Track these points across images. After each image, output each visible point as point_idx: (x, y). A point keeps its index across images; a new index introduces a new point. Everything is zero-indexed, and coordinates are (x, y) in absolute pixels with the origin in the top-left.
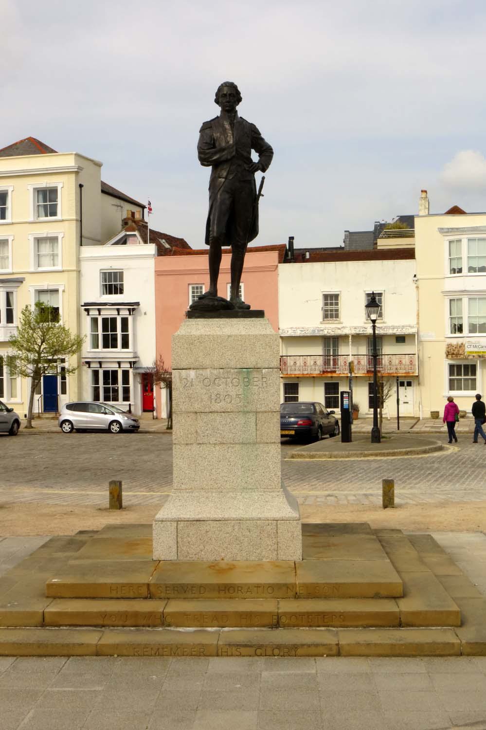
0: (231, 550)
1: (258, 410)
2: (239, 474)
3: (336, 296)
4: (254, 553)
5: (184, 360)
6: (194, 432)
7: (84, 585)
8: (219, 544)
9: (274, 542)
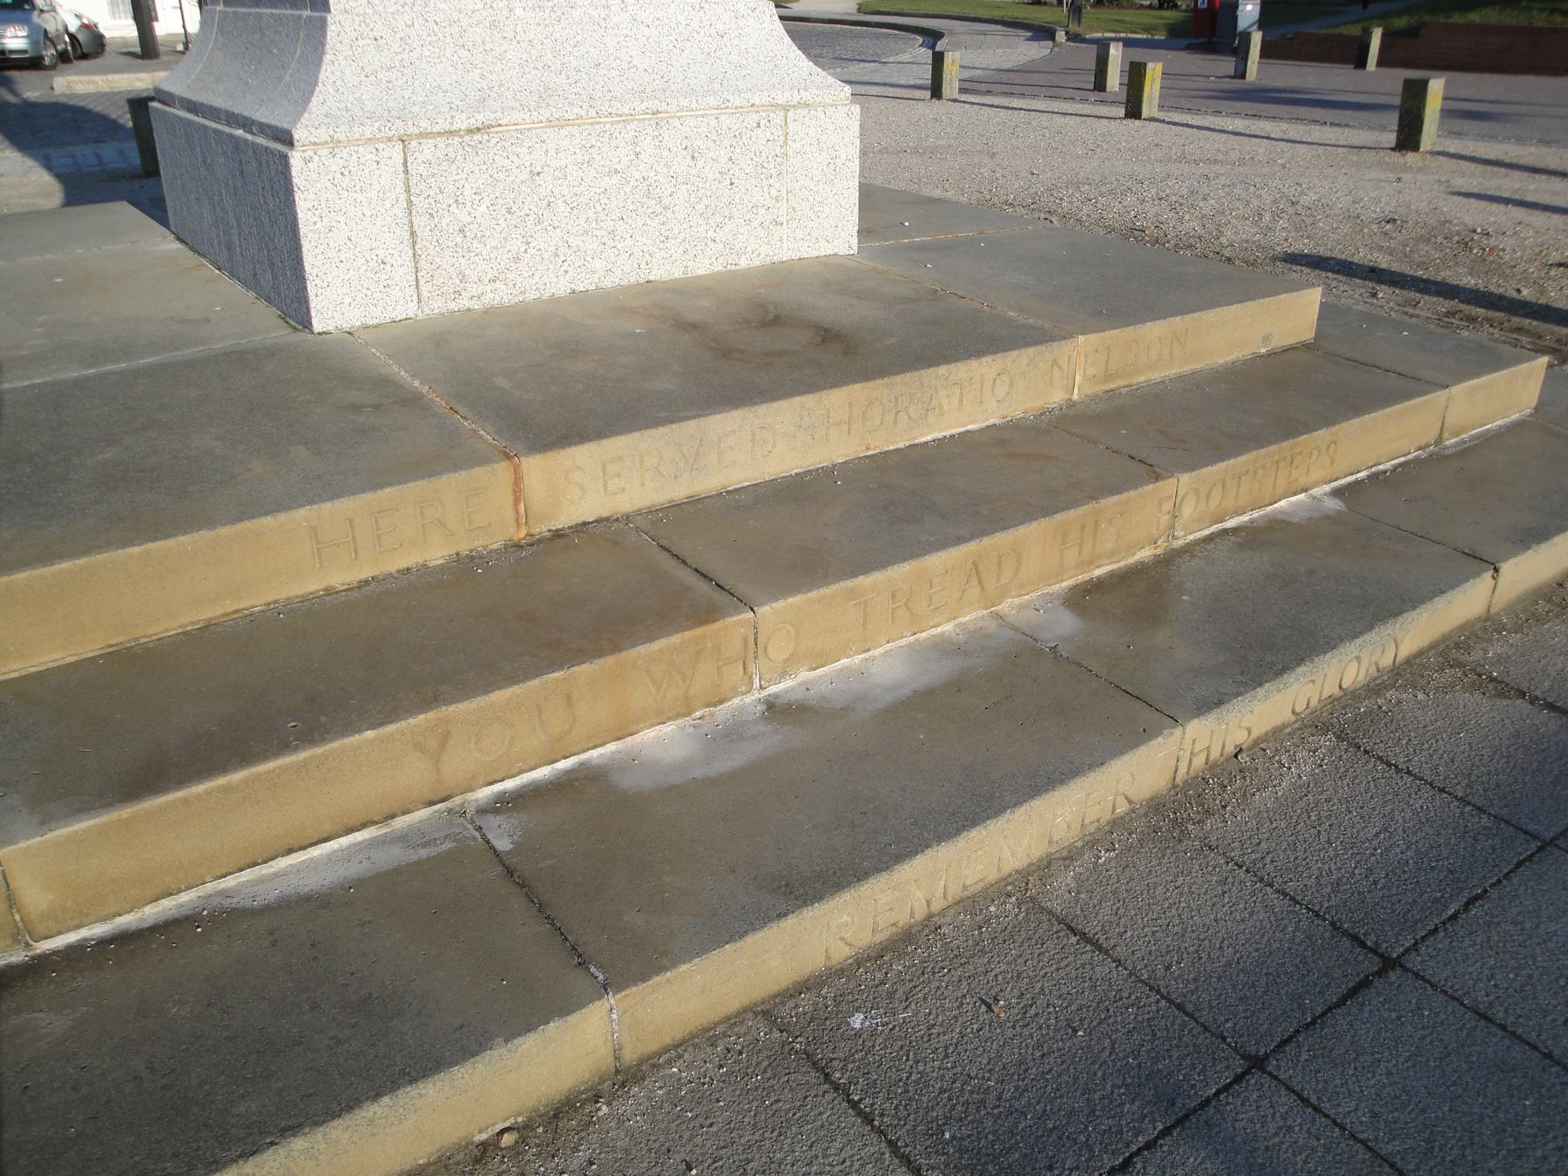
0: (629, 242)
4: (711, 244)
8: (582, 221)
9: (774, 193)
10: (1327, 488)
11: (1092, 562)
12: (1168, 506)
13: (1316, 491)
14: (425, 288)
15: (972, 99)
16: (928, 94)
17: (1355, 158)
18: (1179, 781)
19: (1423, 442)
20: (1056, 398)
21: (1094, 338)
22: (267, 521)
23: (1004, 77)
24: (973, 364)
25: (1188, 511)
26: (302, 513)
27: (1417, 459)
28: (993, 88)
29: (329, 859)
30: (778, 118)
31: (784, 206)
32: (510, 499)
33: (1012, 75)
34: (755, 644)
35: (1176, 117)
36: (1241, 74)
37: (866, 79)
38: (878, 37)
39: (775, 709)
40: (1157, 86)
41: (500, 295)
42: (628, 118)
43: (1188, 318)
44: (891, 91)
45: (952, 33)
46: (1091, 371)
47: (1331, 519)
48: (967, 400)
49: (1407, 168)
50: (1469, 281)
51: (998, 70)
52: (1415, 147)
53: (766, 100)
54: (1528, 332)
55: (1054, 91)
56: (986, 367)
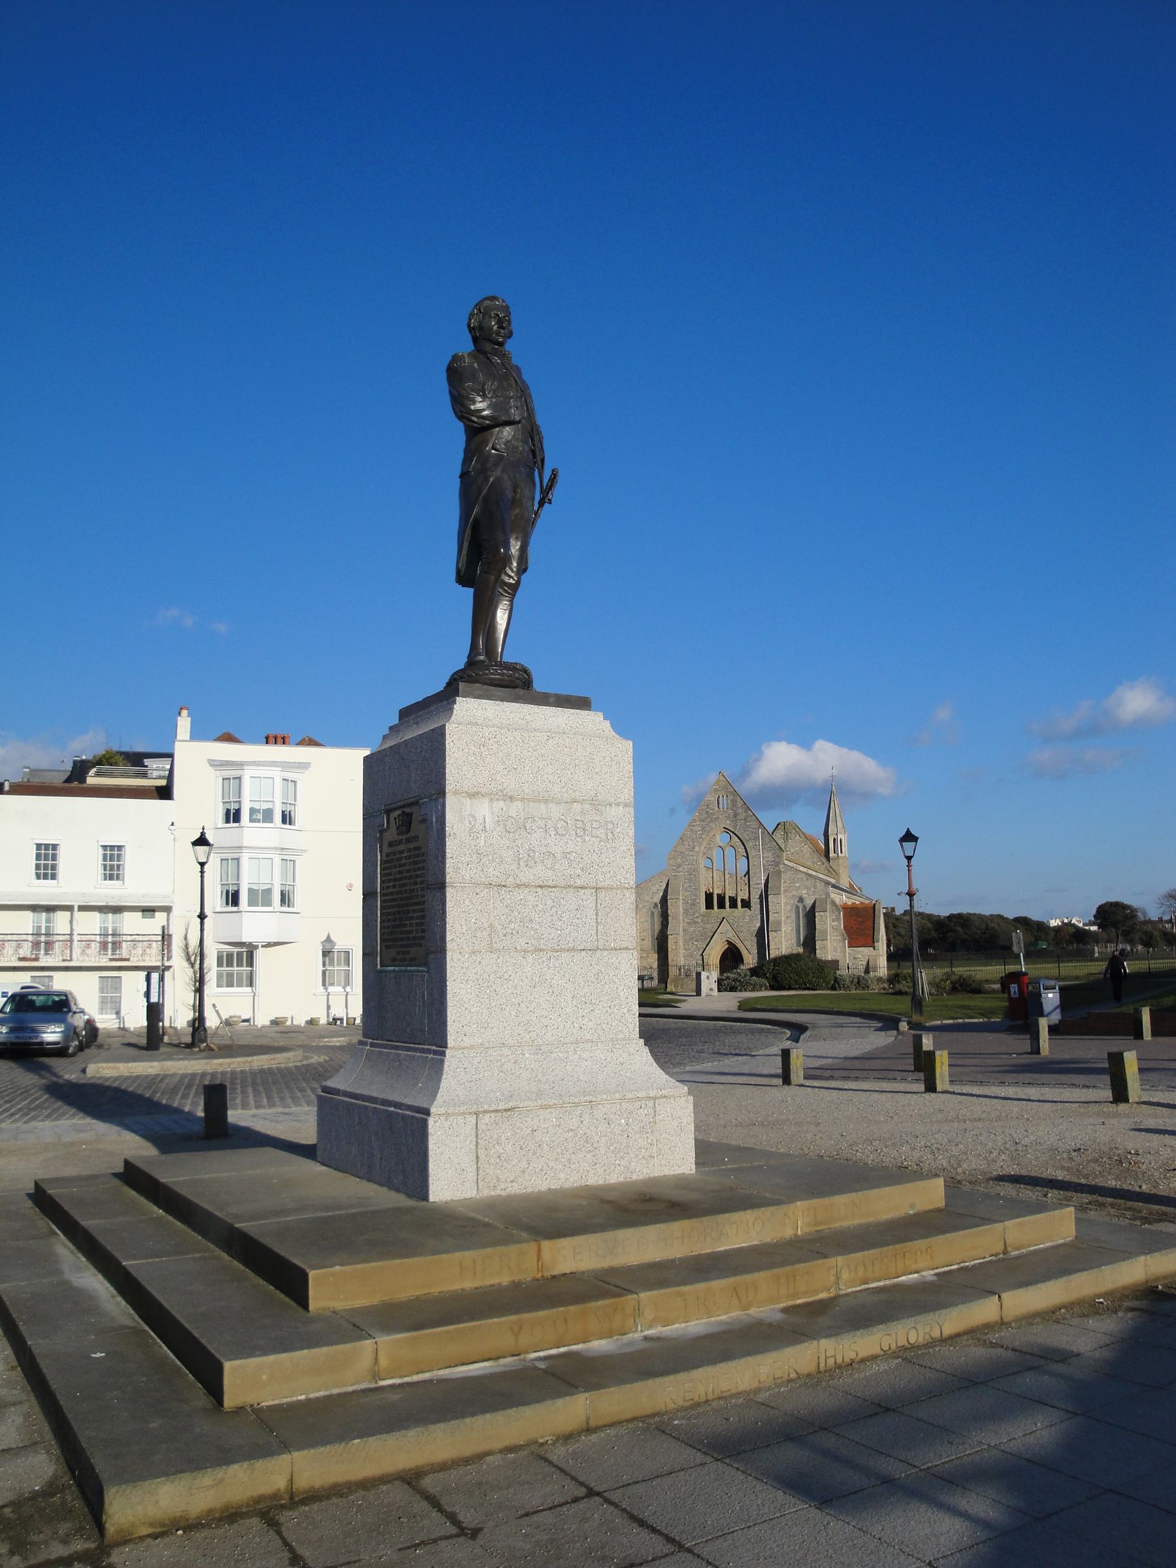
1: (600, 885)
2: (568, 1010)
3: (55, 847)
5: (469, 776)
6: (486, 925)
7: (5, 1307)
10: (932, 1272)
11: (795, 1296)
12: (833, 1272)
13: (924, 1273)
14: (481, 1184)
15: (816, 1083)
16: (780, 1081)
17: (1082, 1110)
18: (822, 1369)
19: (994, 1252)
20: (788, 1233)
21: (806, 1203)
22: (445, 1256)
23: (848, 1064)
24: (742, 1213)
25: (845, 1275)
26: (458, 1254)
27: (991, 1262)
28: (836, 1074)
29: (484, 1368)
30: (651, 1104)
31: (655, 1148)
32: (535, 1258)
33: (856, 1062)
34: (638, 1311)
35: (966, 1089)
36: (1036, 1050)
37: (736, 1070)
38: (752, 1032)
39: (646, 1338)
40: (946, 1067)
41: (515, 1189)
42: (577, 1105)
43: (860, 1193)
44: (760, 1080)
45: (815, 1026)
46: (806, 1220)
47: (931, 1283)
48: (741, 1231)
49: (1117, 1115)
50: (1112, 1183)
51: (845, 1058)
52: (1126, 1100)
53: (644, 1095)
54: (1130, 1209)
55: (885, 1074)
56: (748, 1216)
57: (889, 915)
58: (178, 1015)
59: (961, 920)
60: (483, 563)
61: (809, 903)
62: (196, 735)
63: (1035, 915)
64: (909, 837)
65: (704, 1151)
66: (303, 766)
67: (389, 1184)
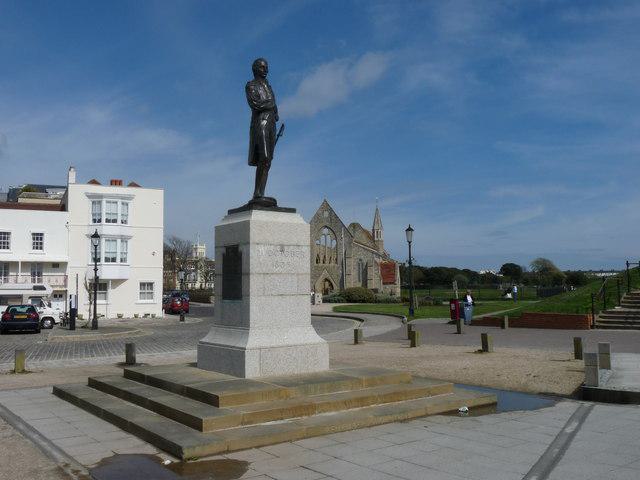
55: (398, 340)
57: (402, 268)
58: (84, 312)
59: (437, 271)
60: (260, 158)
61: (365, 262)
62: (78, 181)
63: (473, 269)
64: (410, 229)
65: (332, 363)
66: (130, 198)
67: (228, 373)
